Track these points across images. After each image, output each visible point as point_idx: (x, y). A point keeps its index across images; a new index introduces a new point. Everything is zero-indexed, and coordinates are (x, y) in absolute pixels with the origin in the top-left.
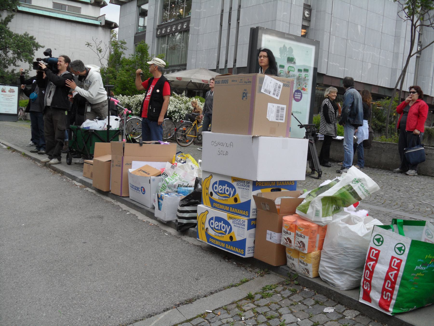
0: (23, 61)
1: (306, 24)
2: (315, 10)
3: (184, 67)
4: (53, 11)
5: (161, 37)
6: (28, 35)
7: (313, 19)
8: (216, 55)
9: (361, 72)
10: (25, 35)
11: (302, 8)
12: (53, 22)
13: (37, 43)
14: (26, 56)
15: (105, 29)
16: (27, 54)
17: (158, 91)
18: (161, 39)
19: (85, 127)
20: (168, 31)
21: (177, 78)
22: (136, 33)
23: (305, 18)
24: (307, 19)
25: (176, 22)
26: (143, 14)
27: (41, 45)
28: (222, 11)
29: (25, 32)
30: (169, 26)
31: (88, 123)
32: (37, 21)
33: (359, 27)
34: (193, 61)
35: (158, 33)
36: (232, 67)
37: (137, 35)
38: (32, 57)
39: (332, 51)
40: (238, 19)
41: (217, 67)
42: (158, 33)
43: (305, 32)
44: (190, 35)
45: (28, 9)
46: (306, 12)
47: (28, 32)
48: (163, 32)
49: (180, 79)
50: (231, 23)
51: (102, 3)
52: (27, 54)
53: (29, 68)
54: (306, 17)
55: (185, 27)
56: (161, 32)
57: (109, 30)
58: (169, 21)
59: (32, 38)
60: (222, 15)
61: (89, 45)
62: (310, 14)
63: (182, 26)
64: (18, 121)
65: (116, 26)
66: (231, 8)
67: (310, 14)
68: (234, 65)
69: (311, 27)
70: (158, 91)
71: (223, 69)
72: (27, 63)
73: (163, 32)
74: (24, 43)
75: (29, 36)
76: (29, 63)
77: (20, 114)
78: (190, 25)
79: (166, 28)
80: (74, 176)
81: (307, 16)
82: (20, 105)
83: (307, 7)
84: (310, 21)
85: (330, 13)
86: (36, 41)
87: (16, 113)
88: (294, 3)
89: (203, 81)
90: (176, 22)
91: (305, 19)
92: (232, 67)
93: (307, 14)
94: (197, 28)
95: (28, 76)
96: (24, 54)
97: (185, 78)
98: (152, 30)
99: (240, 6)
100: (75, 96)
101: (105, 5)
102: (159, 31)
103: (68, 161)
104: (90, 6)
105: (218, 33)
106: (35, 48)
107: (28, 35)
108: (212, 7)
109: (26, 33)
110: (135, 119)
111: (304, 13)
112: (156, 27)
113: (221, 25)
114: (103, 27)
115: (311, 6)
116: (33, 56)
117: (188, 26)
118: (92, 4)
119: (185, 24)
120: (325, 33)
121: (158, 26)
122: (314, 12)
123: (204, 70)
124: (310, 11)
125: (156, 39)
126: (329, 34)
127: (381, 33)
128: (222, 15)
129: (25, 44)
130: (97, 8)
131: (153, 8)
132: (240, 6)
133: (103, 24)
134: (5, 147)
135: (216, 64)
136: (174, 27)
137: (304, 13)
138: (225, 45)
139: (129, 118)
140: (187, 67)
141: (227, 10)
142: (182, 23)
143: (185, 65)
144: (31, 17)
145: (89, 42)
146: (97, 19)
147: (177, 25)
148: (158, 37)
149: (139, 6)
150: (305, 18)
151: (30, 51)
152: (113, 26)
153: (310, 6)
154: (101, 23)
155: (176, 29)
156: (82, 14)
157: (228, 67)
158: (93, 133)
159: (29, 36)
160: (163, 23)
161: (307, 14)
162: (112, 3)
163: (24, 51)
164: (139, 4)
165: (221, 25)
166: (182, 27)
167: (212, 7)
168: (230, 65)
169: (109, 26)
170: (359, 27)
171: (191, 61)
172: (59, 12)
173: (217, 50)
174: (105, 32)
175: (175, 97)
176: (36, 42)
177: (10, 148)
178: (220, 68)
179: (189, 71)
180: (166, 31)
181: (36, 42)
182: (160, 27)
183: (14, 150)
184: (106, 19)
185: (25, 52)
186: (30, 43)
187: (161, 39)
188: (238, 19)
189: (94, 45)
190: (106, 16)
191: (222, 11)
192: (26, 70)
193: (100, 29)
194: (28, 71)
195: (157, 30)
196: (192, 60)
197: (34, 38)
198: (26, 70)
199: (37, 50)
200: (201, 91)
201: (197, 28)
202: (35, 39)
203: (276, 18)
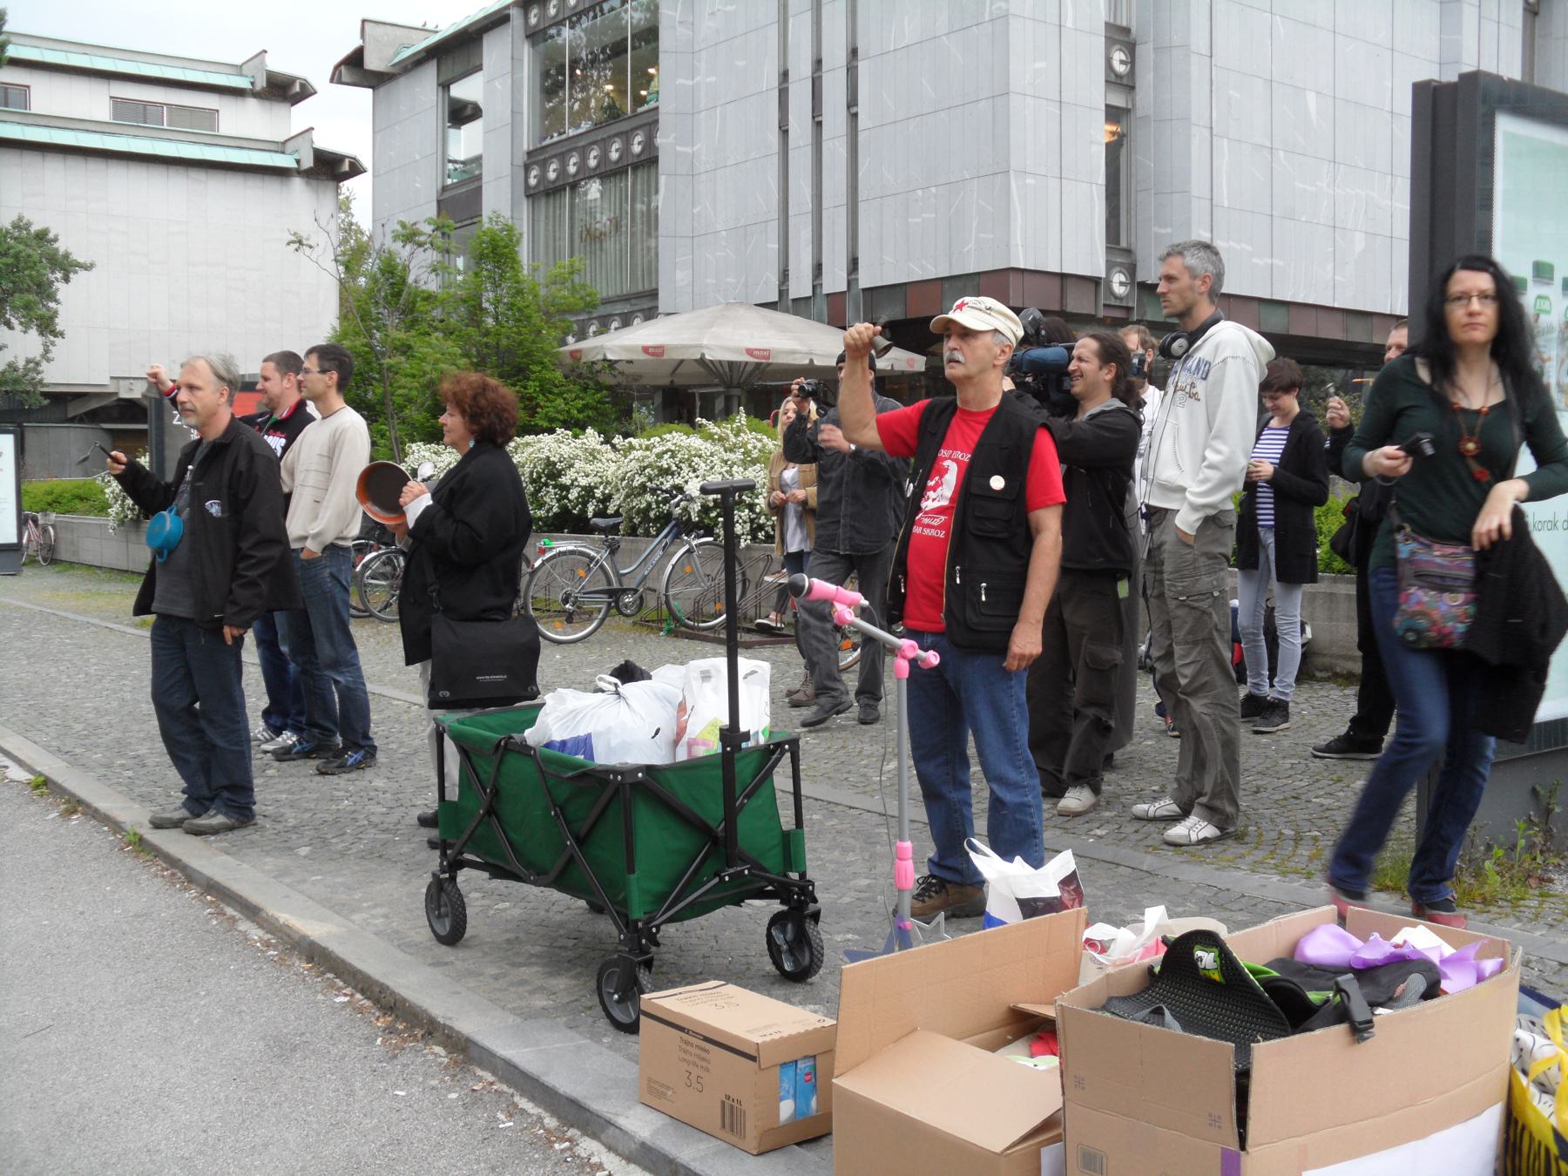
0: (18, 327)
1: (1119, 101)
2: (1151, 45)
3: (646, 304)
4: (114, 129)
5: (543, 194)
6: (28, 225)
7: (1145, 80)
8: (774, 246)
9: (1330, 267)
10: (16, 226)
11: (1100, 42)
12: (119, 175)
13: (66, 256)
14: (27, 307)
15: (314, 182)
16: (32, 297)
17: (997, 483)
18: (543, 201)
19: (557, 736)
20: (572, 169)
21: (646, 349)
22: (445, 189)
23: (1113, 78)
24: (1122, 83)
25: (600, 135)
26: (461, 114)
27: (81, 260)
28: (785, 75)
29: (14, 217)
30: (574, 149)
31: (574, 713)
32: (54, 172)
33: (1311, 98)
34: (682, 277)
35: (533, 182)
36: (844, 288)
37: (447, 195)
38: (49, 309)
39: (1224, 197)
40: (852, 102)
41: (783, 293)
42: (533, 182)
43: (1113, 133)
44: (662, 179)
45: (19, 128)
46: (1118, 56)
47: (27, 217)
48: (552, 175)
49: (655, 351)
50: (826, 119)
51: (297, 88)
52: (32, 297)
53: (41, 350)
54: (1118, 76)
55: (637, 149)
56: (542, 177)
57: (332, 184)
58: (571, 132)
59: (42, 236)
60: (783, 94)
61: (300, 242)
62: (1132, 62)
63: (628, 144)
64: (27, 571)
65: (356, 169)
66: (818, 63)
67: (1132, 62)
68: (851, 283)
69: (1140, 112)
70: (997, 483)
71: (808, 298)
72: (33, 332)
73: (552, 175)
74: (17, 256)
75: (33, 229)
76: (41, 334)
77: (29, 540)
78: (659, 141)
79: (563, 158)
80: (573, 1103)
81: (1121, 69)
82: (25, 505)
83: (1120, 36)
84: (1131, 88)
85: (1206, 51)
86: (61, 246)
87: (14, 540)
88: (1069, 23)
89: (750, 352)
90: (600, 135)
91: (1118, 82)
92: (844, 288)
93: (1122, 62)
94: (689, 150)
95: (40, 382)
96: (18, 299)
97: (781, 352)
98: (507, 170)
99: (854, 53)
100: (419, 521)
101: (306, 92)
102: (534, 173)
103: (445, 928)
104: (252, 103)
105: (774, 163)
106: (59, 275)
107: (28, 225)
108: (740, 63)
109: (20, 219)
110: (572, 552)
111: (1109, 61)
112: (521, 159)
113: (784, 132)
114: (308, 174)
115: (1133, 30)
116: (52, 305)
117: (649, 144)
118: (256, 94)
119: (638, 139)
120: (1194, 130)
121: (529, 154)
122: (1145, 53)
123: (741, 311)
124: (1131, 48)
125: (525, 205)
126: (1207, 133)
127: (1389, 116)
128: (783, 94)
129: (18, 264)
130: (279, 109)
131: (503, 86)
132: (854, 53)
133: (308, 162)
134: (16, 773)
135: (774, 280)
136: (594, 153)
137: (1109, 61)
138: (808, 206)
139: (543, 552)
140: (663, 303)
141: (801, 70)
142: (627, 137)
143: (653, 294)
144: (31, 159)
145: (304, 235)
146: (281, 147)
147: (604, 144)
148: (531, 195)
149: (445, 86)
150: (1113, 78)
151: (39, 285)
152: (346, 167)
153: (1127, 31)
154: (298, 162)
155: (582, 164)
156: (222, 132)
157: (827, 289)
158: (638, 786)
159: (33, 229)
160: (548, 141)
161: (1122, 62)
162: (340, 82)
163: (17, 289)
164: (443, 78)
165: (784, 132)
166: (625, 151)
167: (740, 63)
168: (835, 281)
169: (330, 169)
170: (1311, 98)
171: (674, 279)
172: (136, 131)
173: (774, 228)
174: (317, 192)
175: (709, 437)
176: (62, 251)
177: (45, 785)
178: (792, 295)
179: (704, 311)
180: (562, 171)
181: (62, 251)
182: (535, 158)
183: (75, 805)
184: (318, 145)
185: (21, 291)
186: (36, 257)
187: (543, 201)
188: (852, 102)
189: (322, 245)
190: (314, 134)
191: (785, 75)
192: (28, 361)
193: (297, 183)
194: (38, 364)
195: (527, 168)
196: (679, 275)
197: (51, 236)
198: (28, 361)
199: (67, 280)
200: (736, 392)
201: (689, 150)
202: (56, 240)
203: (1008, 84)
